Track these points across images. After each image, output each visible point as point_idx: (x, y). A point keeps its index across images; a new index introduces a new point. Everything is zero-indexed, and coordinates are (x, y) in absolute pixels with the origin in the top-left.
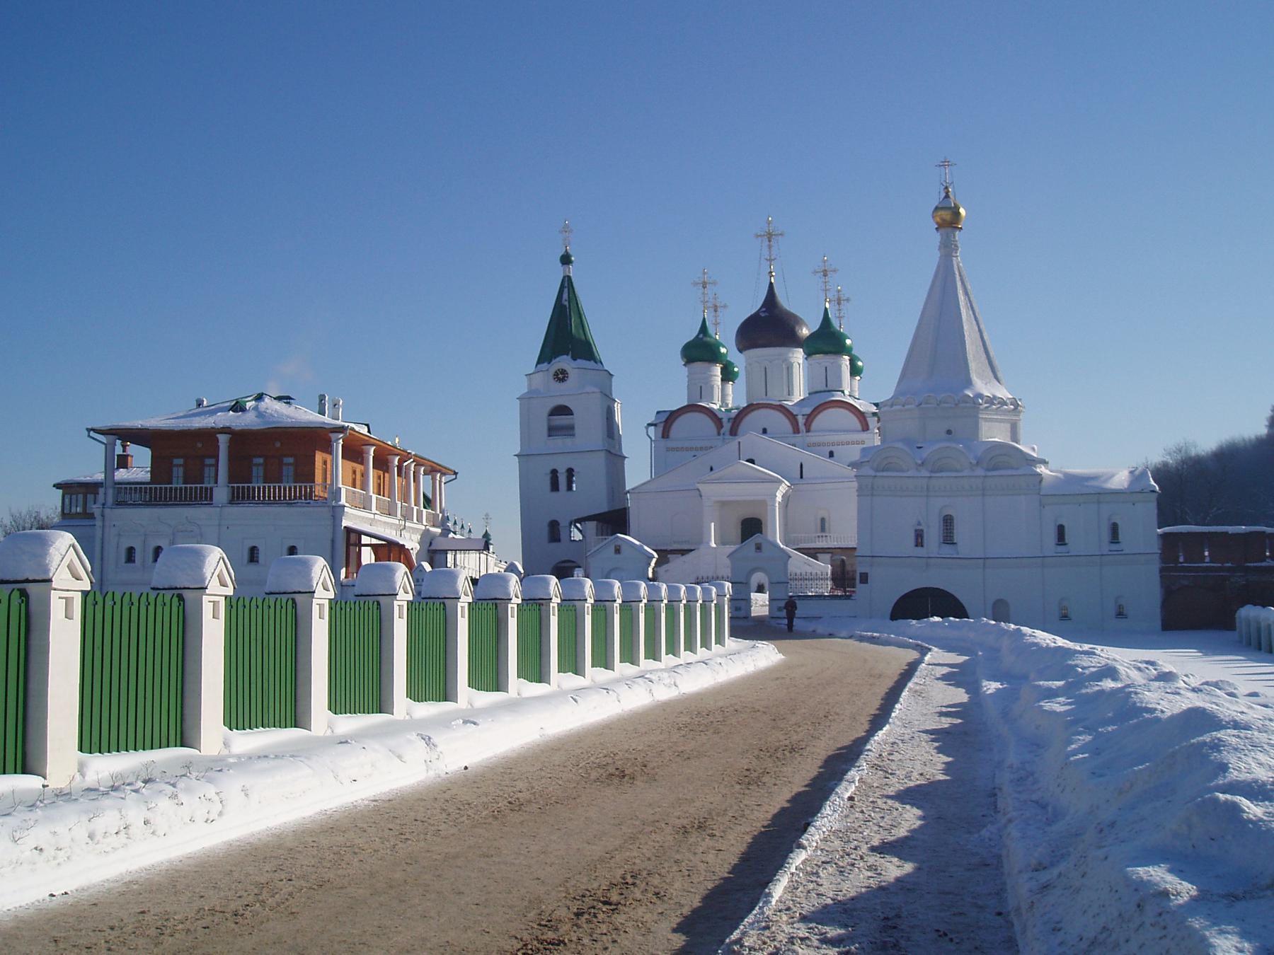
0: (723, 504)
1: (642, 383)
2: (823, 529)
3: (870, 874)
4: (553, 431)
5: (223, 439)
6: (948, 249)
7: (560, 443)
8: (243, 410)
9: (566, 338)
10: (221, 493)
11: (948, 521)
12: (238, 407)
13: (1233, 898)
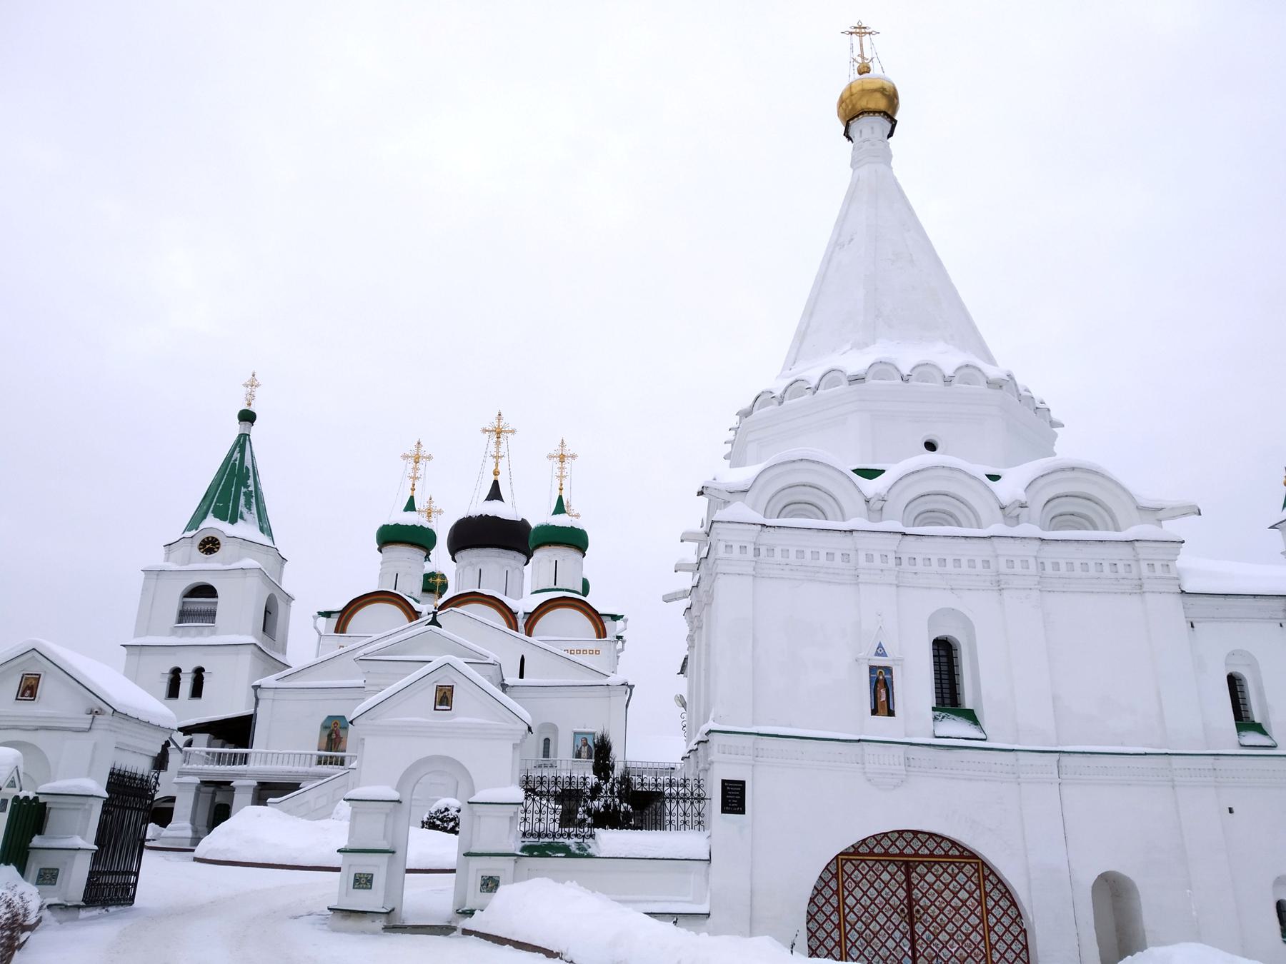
2: (546, 753)
4: (184, 616)
7: (196, 635)
9: (234, 489)
11: (945, 651)
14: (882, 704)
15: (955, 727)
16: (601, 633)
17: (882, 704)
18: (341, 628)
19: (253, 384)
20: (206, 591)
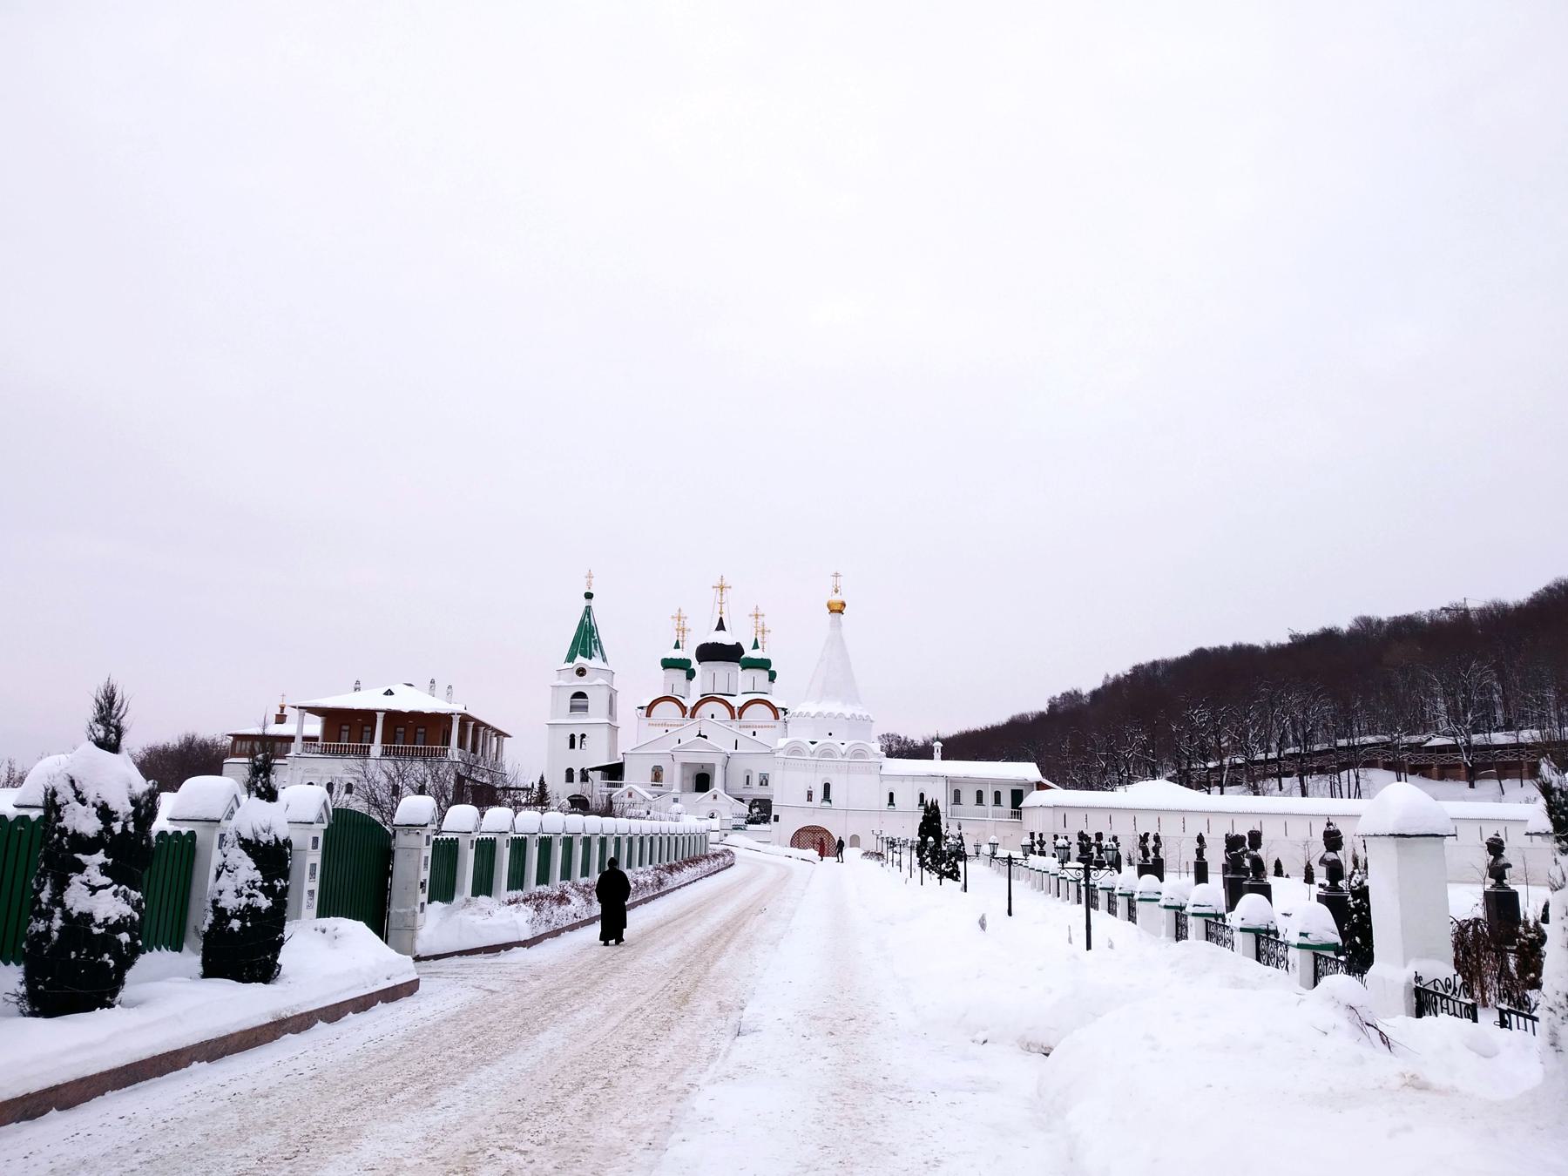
0: (684, 765)
1: (631, 665)
3: (631, 665)
4: (573, 708)
5: (380, 716)
7: (579, 718)
9: (586, 640)
10: (376, 749)
11: (827, 787)
14: (810, 799)
15: (826, 804)
16: (777, 717)
17: (810, 799)
18: (648, 715)
19: (590, 576)
20: (580, 695)
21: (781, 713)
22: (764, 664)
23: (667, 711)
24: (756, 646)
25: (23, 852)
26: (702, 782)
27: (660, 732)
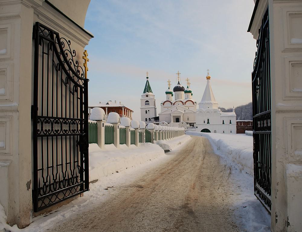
0: (173, 116)
1: (159, 96)
3: (159, 96)
4: (146, 104)
6: (208, 82)
7: (147, 106)
8: (108, 104)
9: (148, 89)
11: (208, 120)
12: (108, 104)
13: (194, 144)
14: (204, 123)
17: (204, 123)
19: (147, 73)
21: (195, 103)
22: (190, 92)
23: (168, 104)
24: (188, 87)
25: (15, 2)
26: (178, 120)
27: (166, 109)
